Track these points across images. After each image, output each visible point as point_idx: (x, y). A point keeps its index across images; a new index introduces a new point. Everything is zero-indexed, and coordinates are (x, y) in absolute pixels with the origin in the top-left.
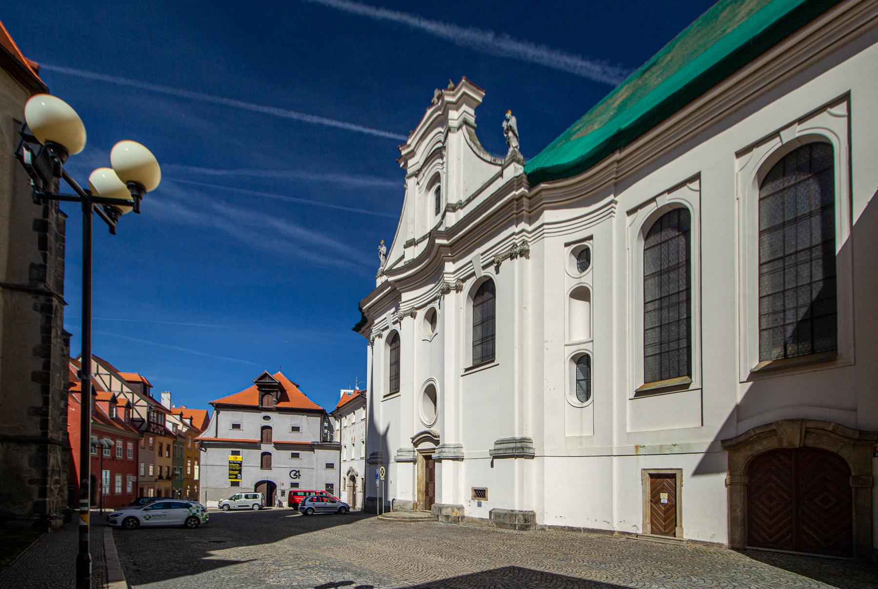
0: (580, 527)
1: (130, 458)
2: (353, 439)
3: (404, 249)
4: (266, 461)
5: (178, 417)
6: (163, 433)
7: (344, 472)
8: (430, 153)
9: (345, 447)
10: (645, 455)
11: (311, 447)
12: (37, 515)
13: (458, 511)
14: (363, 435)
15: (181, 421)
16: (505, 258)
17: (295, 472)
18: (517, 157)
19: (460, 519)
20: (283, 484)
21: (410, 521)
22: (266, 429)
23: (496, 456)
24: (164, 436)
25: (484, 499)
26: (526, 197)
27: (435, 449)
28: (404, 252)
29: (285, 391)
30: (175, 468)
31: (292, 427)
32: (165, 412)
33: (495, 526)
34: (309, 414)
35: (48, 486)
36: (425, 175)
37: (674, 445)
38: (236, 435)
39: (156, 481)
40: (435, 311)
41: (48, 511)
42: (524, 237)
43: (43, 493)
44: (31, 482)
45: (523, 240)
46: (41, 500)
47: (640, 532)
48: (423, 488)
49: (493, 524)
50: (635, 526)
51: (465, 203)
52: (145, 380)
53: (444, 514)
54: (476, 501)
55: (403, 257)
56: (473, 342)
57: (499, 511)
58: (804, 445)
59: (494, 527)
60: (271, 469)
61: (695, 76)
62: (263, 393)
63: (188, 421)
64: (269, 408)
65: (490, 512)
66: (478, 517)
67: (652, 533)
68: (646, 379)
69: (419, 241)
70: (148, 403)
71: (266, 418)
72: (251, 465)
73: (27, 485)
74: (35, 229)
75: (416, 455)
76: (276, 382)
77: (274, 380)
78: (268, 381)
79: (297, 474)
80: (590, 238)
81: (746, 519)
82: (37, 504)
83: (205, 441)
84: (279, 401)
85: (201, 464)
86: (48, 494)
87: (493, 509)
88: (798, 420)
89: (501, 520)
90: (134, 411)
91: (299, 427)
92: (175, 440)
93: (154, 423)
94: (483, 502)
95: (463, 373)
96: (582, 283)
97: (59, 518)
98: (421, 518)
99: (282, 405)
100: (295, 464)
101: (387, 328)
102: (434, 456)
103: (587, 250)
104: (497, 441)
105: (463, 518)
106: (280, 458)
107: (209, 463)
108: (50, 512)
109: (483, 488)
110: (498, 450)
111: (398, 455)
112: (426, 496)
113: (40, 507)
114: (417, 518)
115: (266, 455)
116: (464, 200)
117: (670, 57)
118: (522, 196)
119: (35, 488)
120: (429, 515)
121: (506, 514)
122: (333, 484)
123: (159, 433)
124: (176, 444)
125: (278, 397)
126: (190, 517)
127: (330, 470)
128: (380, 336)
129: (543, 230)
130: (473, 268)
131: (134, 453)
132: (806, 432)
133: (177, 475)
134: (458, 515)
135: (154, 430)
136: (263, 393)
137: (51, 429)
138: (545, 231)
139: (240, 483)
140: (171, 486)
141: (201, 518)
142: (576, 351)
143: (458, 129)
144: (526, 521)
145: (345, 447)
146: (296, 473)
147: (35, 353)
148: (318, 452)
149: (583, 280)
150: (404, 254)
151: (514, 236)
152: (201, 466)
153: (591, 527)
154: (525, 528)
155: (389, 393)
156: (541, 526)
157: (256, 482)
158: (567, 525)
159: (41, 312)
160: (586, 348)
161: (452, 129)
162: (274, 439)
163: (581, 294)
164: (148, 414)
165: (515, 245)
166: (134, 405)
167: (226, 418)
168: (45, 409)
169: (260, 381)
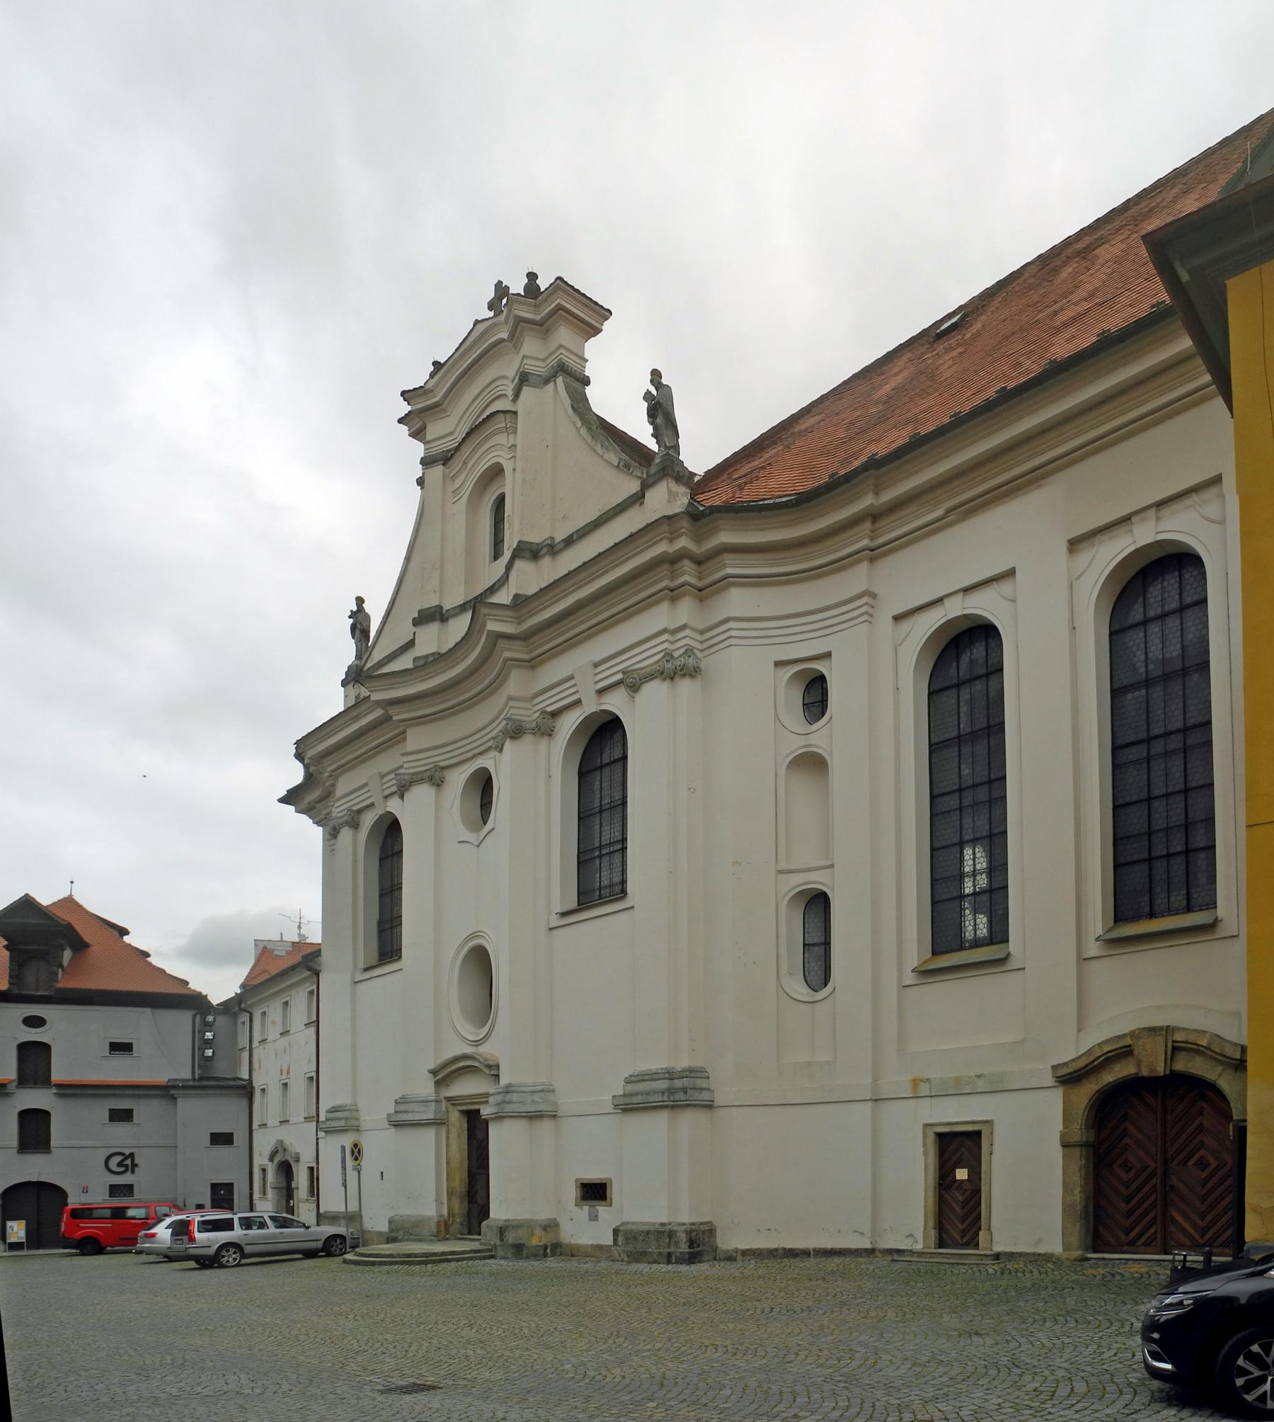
0: (807, 1246)
2: (285, 1072)
3: (414, 629)
7: (260, 1154)
8: (481, 420)
9: (263, 1090)
14: (309, 1060)
16: (649, 677)
18: (674, 470)
19: (548, 1250)
21: (426, 1263)
23: (628, 1107)
25: (604, 1203)
27: (487, 1095)
28: (414, 633)
33: (626, 1259)
36: (469, 466)
37: (978, 1076)
40: (490, 777)
42: (687, 639)
45: (666, 649)
47: (919, 1246)
48: (460, 1182)
49: (622, 1255)
50: (911, 1235)
51: (561, 546)
54: (586, 1208)
55: (411, 644)
57: (634, 1227)
58: (1171, 1070)
59: (623, 1261)
65: (616, 1232)
66: (590, 1243)
67: (940, 1247)
68: (935, 947)
69: (452, 613)
71: (34, 1022)
75: (444, 1109)
79: (128, 1162)
80: (828, 655)
81: (1091, 1206)
87: (623, 1224)
88: (1161, 1028)
89: (640, 1247)
94: (602, 1209)
95: (556, 921)
96: (811, 745)
98: (452, 1253)
100: (121, 1136)
102: (485, 1111)
103: (821, 679)
109: (602, 1179)
110: (631, 1095)
111: (396, 1112)
112: (469, 1203)
114: (443, 1254)
116: (560, 536)
117: (980, 325)
120: (475, 1246)
122: (232, 1184)
128: (354, 824)
129: (730, 629)
130: (596, 683)
132: (1174, 1048)
138: (732, 633)
142: (802, 884)
143: (547, 381)
144: (691, 1243)
145: (263, 1090)
149: (813, 739)
150: (414, 639)
151: (666, 637)
153: (829, 1245)
154: (693, 1258)
156: (727, 1251)
158: (781, 1246)
160: (818, 880)
161: (532, 379)
162: (56, 1076)
163: (812, 763)
165: (669, 656)
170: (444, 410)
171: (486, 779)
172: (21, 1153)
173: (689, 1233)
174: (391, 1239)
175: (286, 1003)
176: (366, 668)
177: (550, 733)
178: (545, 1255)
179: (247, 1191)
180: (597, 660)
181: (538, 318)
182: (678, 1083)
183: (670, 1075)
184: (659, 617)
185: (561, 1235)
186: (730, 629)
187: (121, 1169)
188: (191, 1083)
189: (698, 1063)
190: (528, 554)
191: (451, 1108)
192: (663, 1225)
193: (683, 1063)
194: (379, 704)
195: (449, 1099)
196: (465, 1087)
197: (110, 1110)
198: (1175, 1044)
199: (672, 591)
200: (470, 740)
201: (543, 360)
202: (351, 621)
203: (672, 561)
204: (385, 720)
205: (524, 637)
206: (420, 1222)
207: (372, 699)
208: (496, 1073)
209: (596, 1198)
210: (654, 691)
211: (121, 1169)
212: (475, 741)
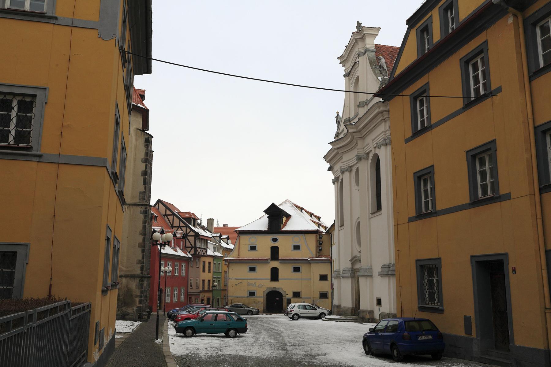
1: (183, 274)
10: (109, 312)
30: (214, 281)
31: (294, 246)
38: (253, 255)
44: (136, 296)
61: (480, 35)
71: (275, 240)
74: (142, 176)
90: (187, 241)
91: (299, 246)
93: (199, 248)
97: (146, 315)
104: (383, 266)
123: (203, 254)
131: (186, 271)
133: (215, 286)
134: (369, 317)
137: (144, 270)
159: (143, 214)
168: (142, 261)
170: (348, 60)
171: (378, 158)
172: (321, 281)
176: (340, 132)
177: (368, 159)
180: (373, 138)
197: (250, 267)
199: (384, 119)
200: (352, 160)
201: (364, 48)
202: (336, 119)
203: (382, 112)
204: (337, 153)
209: (379, 304)
210: (383, 148)
212: (368, 149)
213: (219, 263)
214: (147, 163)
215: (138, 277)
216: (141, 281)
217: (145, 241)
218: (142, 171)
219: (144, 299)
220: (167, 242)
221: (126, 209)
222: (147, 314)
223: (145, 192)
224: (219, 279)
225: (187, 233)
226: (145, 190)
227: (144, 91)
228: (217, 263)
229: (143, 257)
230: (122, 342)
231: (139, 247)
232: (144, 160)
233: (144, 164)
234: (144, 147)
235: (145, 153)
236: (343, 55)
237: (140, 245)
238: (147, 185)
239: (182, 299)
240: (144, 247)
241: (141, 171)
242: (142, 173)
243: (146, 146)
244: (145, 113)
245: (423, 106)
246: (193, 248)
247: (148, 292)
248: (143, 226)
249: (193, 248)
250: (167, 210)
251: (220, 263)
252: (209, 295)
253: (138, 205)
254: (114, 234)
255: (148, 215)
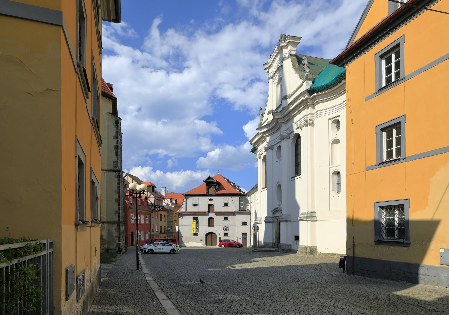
4: (210, 222)
5: (169, 200)
6: (162, 210)
11: (234, 214)
12: (118, 248)
13: (288, 247)
15: (171, 202)
17: (226, 228)
19: (289, 251)
20: (220, 234)
22: (210, 206)
24: (162, 211)
26: (309, 99)
29: (221, 184)
31: (224, 204)
32: (162, 199)
34: (232, 196)
35: (121, 238)
36: (277, 78)
38: (195, 210)
39: (159, 234)
41: (121, 247)
43: (119, 241)
46: (119, 243)
52: (153, 184)
53: (282, 248)
54: (296, 242)
56: (296, 164)
60: (214, 226)
62: (209, 187)
63: (174, 201)
64: (212, 195)
70: (154, 196)
71: (210, 200)
72: (203, 224)
73: (115, 238)
74: (114, 149)
76: (215, 181)
77: (214, 180)
78: (211, 180)
79: (227, 229)
80: (339, 116)
82: (118, 244)
83: (180, 213)
84: (217, 190)
85: (179, 225)
86: (121, 241)
92: (168, 212)
93: (157, 205)
97: (124, 249)
98: (271, 250)
99: (220, 192)
100: (226, 223)
101: (263, 154)
105: (291, 250)
106: (219, 220)
107: (183, 225)
108: (121, 247)
113: (118, 245)
114: (269, 250)
115: (210, 220)
118: (306, 99)
119: (117, 239)
121: (303, 248)
123: (160, 210)
124: (168, 214)
125: (217, 188)
126: (172, 249)
127: (245, 226)
128: (260, 158)
129: (318, 113)
133: (169, 230)
134: (288, 249)
135: (157, 209)
136: (209, 187)
138: (319, 114)
139: (198, 234)
140: (167, 236)
141: (176, 250)
142: (335, 170)
143: (288, 58)
144: (311, 251)
146: (227, 228)
147: (116, 192)
148: (238, 216)
149: (337, 136)
151: (306, 117)
152: (179, 226)
155: (265, 187)
157: (206, 233)
164: (155, 201)
166: (148, 197)
167: (191, 201)
168: (119, 211)
169: (206, 181)
173: (310, 248)
174: (264, 247)
175: (255, 194)
178: (288, 252)
179: (250, 235)
181: (285, 45)
182: (309, 215)
183: (307, 213)
184: (306, 112)
185: (292, 248)
186: (318, 113)
187: (226, 230)
188: (239, 212)
189: (313, 211)
190: (284, 98)
191: (275, 219)
192: (306, 246)
193: (310, 211)
194: (261, 133)
195: (275, 217)
196: (277, 215)
198: (163, 232)
200: (276, 140)
204: (262, 136)
205: (284, 117)
206: (269, 243)
207: (259, 133)
208: (281, 212)
211: (226, 230)
213: (171, 215)
214: (118, 139)
215: (116, 223)
216: (119, 226)
217: (120, 197)
218: (115, 146)
219: (122, 238)
220: (142, 191)
221: (104, 174)
222: (125, 248)
223: (118, 161)
224: (171, 226)
225: (149, 196)
226: (118, 159)
227: (112, 85)
228: (170, 215)
229: (119, 209)
230: (107, 273)
231: (115, 201)
232: (115, 137)
233: (116, 141)
234: (115, 127)
235: (116, 131)
236: (268, 62)
237: (116, 200)
238: (119, 156)
239: (147, 238)
240: (120, 201)
241: (114, 146)
242: (114, 147)
243: (116, 127)
244: (114, 101)
245: (391, 62)
246: (153, 206)
247: (124, 233)
248: (118, 186)
249: (153, 206)
250: (133, 180)
251: (172, 215)
252: (165, 235)
253: (113, 171)
254: (76, 134)
255: (121, 179)
